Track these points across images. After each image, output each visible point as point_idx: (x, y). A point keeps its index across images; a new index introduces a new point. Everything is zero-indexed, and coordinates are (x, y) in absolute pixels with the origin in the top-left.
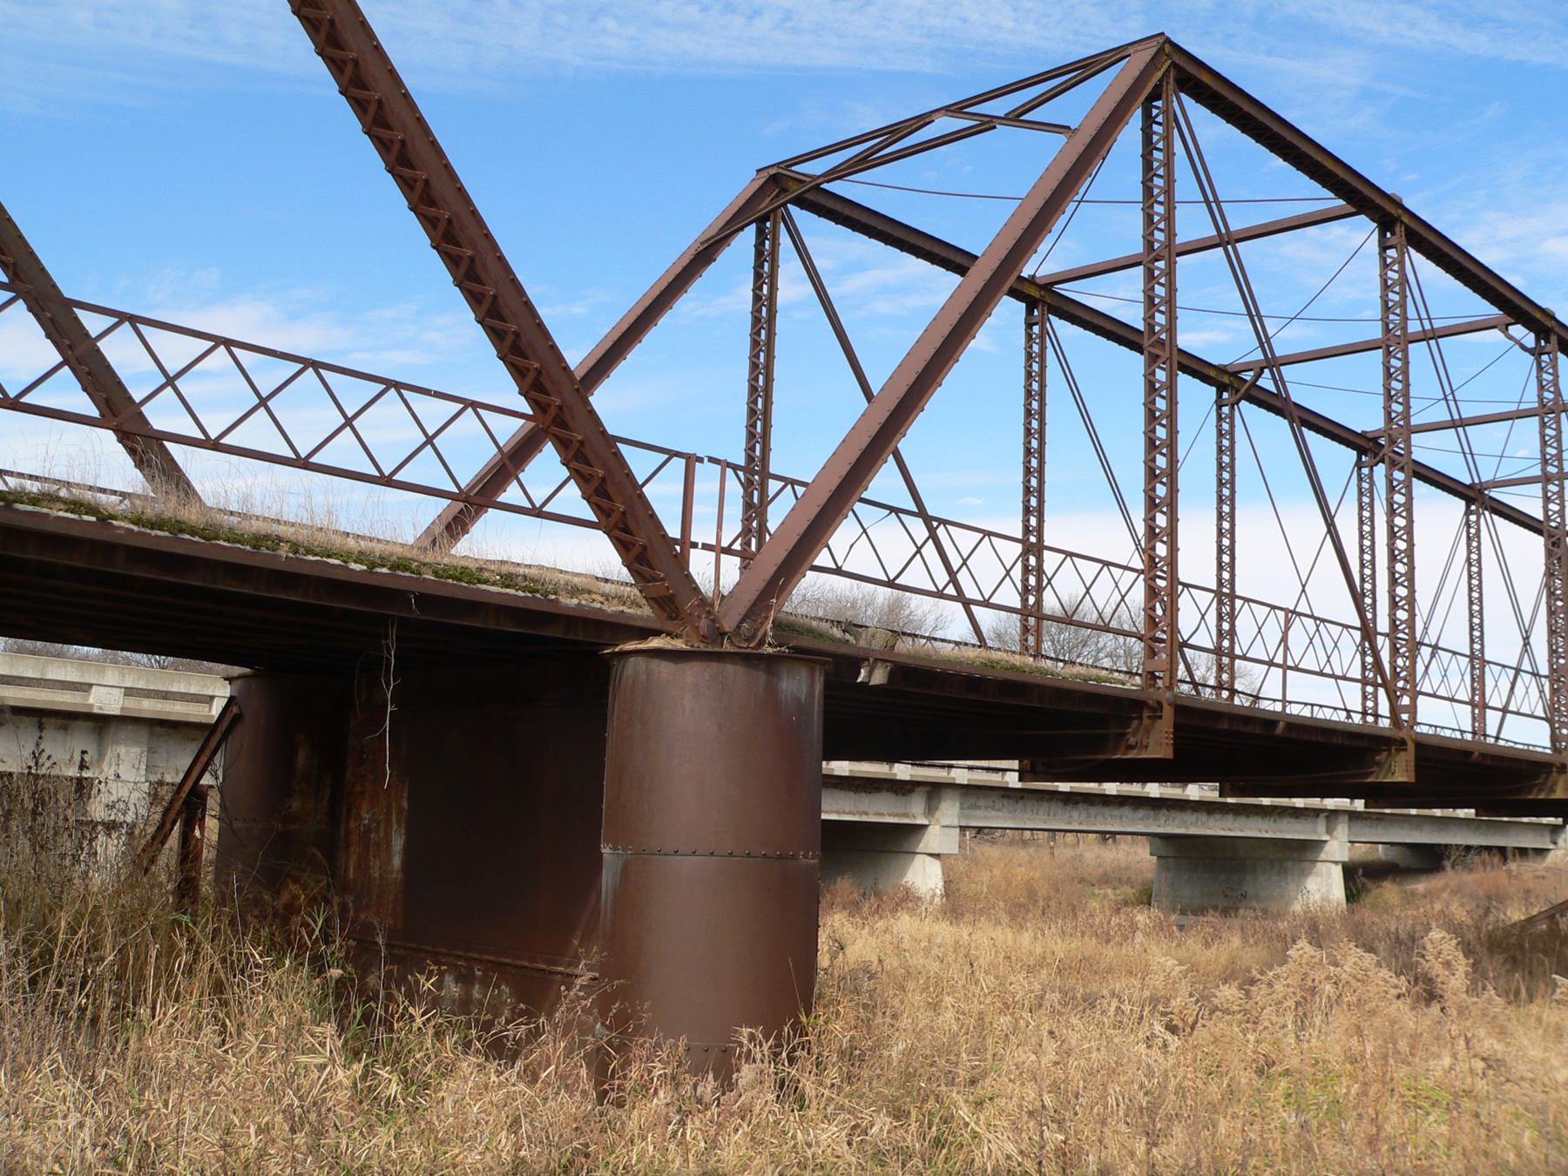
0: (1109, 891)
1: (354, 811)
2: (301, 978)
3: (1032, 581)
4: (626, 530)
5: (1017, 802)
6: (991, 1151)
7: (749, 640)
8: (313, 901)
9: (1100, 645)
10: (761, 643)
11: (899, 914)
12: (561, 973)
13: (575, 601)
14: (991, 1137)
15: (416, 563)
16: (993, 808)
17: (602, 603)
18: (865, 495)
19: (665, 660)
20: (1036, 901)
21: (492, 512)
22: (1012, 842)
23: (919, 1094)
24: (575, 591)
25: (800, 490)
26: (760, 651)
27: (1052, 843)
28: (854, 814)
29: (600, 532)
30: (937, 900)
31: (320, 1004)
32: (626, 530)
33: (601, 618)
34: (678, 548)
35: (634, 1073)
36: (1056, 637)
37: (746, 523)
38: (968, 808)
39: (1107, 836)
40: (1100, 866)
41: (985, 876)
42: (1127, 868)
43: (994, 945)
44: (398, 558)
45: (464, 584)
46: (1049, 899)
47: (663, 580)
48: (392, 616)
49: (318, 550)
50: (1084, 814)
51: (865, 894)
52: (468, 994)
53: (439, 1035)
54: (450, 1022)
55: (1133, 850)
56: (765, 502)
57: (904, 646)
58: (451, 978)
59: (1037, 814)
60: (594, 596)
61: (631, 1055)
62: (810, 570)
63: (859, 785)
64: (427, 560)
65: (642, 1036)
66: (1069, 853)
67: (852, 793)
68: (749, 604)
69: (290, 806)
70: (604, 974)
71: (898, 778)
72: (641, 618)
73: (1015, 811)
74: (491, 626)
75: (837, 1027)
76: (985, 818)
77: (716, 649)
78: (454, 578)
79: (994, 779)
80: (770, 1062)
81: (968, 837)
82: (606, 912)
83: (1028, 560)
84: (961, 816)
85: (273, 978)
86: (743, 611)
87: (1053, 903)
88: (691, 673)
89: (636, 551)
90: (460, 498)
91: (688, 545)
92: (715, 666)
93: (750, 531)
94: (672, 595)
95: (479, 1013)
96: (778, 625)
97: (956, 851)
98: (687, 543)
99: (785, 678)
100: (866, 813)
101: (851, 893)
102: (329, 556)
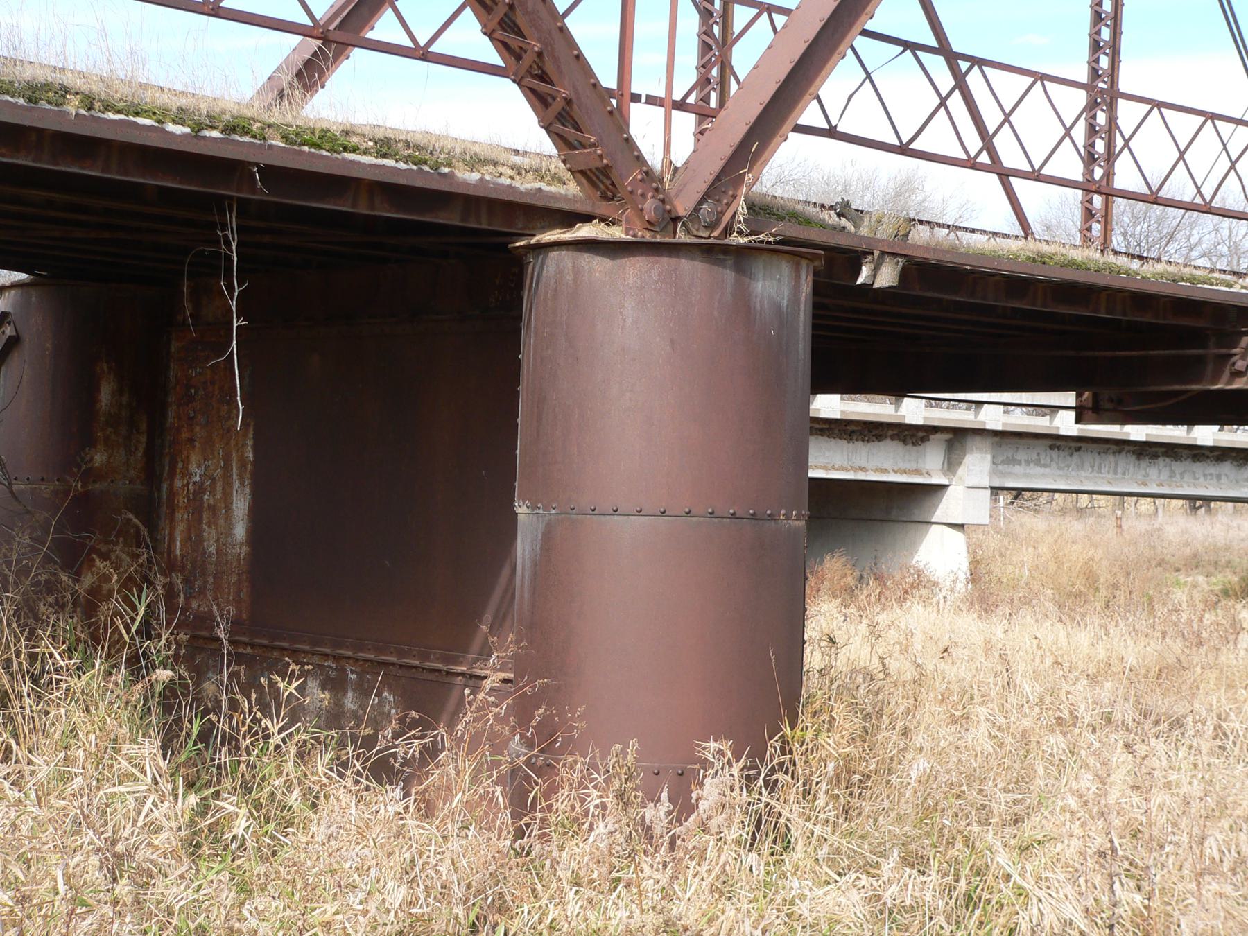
0: (1201, 579)
1: (180, 465)
2: (116, 684)
3: (1100, 146)
4: (543, 77)
5: (1071, 455)
6: (1042, 914)
7: (711, 227)
8: (128, 583)
9: (1193, 240)
10: (728, 231)
11: (909, 604)
12: (462, 674)
13: (475, 176)
14: (1042, 894)
15: (259, 125)
16: (1038, 463)
17: (512, 178)
18: (870, 26)
19: (597, 254)
20: (1097, 590)
21: (357, 53)
22: (1063, 511)
23: (941, 835)
24: (475, 162)
25: (780, 20)
26: (727, 241)
27: (1119, 513)
28: (847, 470)
29: (508, 81)
30: (960, 586)
31: (141, 718)
32: (543, 77)
33: (512, 199)
34: (614, 102)
35: (562, 802)
36: (1129, 231)
37: (703, 70)
38: (1003, 462)
39: (1198, 503)
40: (1187, 544)
41: (1027, 555)
42: (1228, 548)
43: (1039, 647)
44: (233, 117)
45: (325, 153)
46: (1116, 586)
47: (594, 145)
48: (230, 198)
49: (121, 105)
50: (1165, 474)
51: (861, 577)
52: (338, 704)
53: (303, 755)
54: (316, 739)
55: (1235, 524)
56: (727, 41)
57: (921, 235)
58: (316, 683)
59: (1100, 471)
60: (501, 169)
61: (558, 779)
62: (793, 131)
63: (853, 432)
64: (272, 120)
65: (571, 753)
66: (1143, 526)
67: (845, 442)
68: (711, 178)
69: (92, 459)
70: (520, 673)
71: (907, 421)
72: (565, 198)
73: (1068, 466)
74: (363, 210)
75: (831, 742)
76: (1027, 476)
77: (667, 240)
78: (313, 145)
79: (1039, 423)
80: (741, 788)
81: (1002, 503)
82: (522, 592)
83: (1094, 117)
84: (994, 473)
85: (78, 684)
86: (703, 187)
87: (1120, 594)
88: (635, 269)
89: (557, 106)
90: (315, 33)
91: (627, 97)
92: (665, 262)
93: (708, 81)
94: (607, 166)
95: (357, 726)
96: (751, 206)
97: (986, 521)
98: (625, 94)
99: (761, 276)
100: (863, 469)
101: (845, 576)
102: (137, 114)
